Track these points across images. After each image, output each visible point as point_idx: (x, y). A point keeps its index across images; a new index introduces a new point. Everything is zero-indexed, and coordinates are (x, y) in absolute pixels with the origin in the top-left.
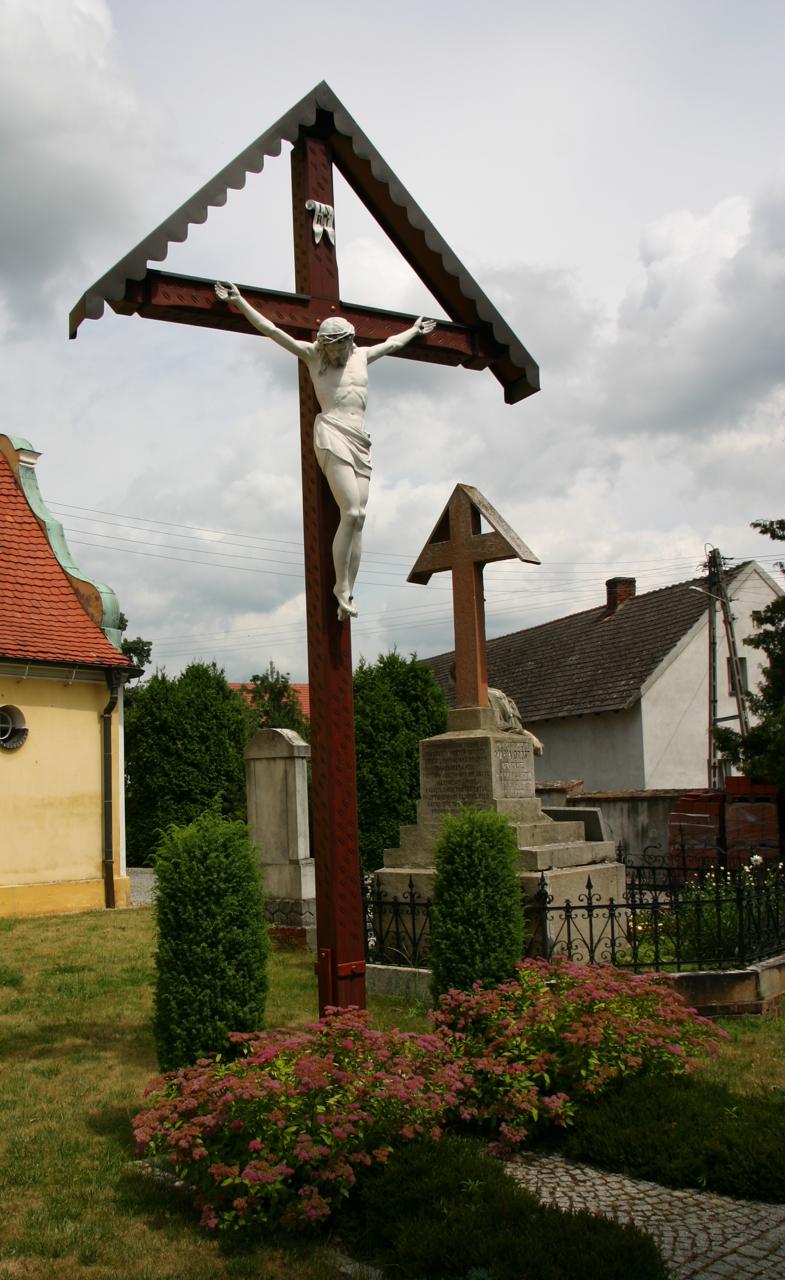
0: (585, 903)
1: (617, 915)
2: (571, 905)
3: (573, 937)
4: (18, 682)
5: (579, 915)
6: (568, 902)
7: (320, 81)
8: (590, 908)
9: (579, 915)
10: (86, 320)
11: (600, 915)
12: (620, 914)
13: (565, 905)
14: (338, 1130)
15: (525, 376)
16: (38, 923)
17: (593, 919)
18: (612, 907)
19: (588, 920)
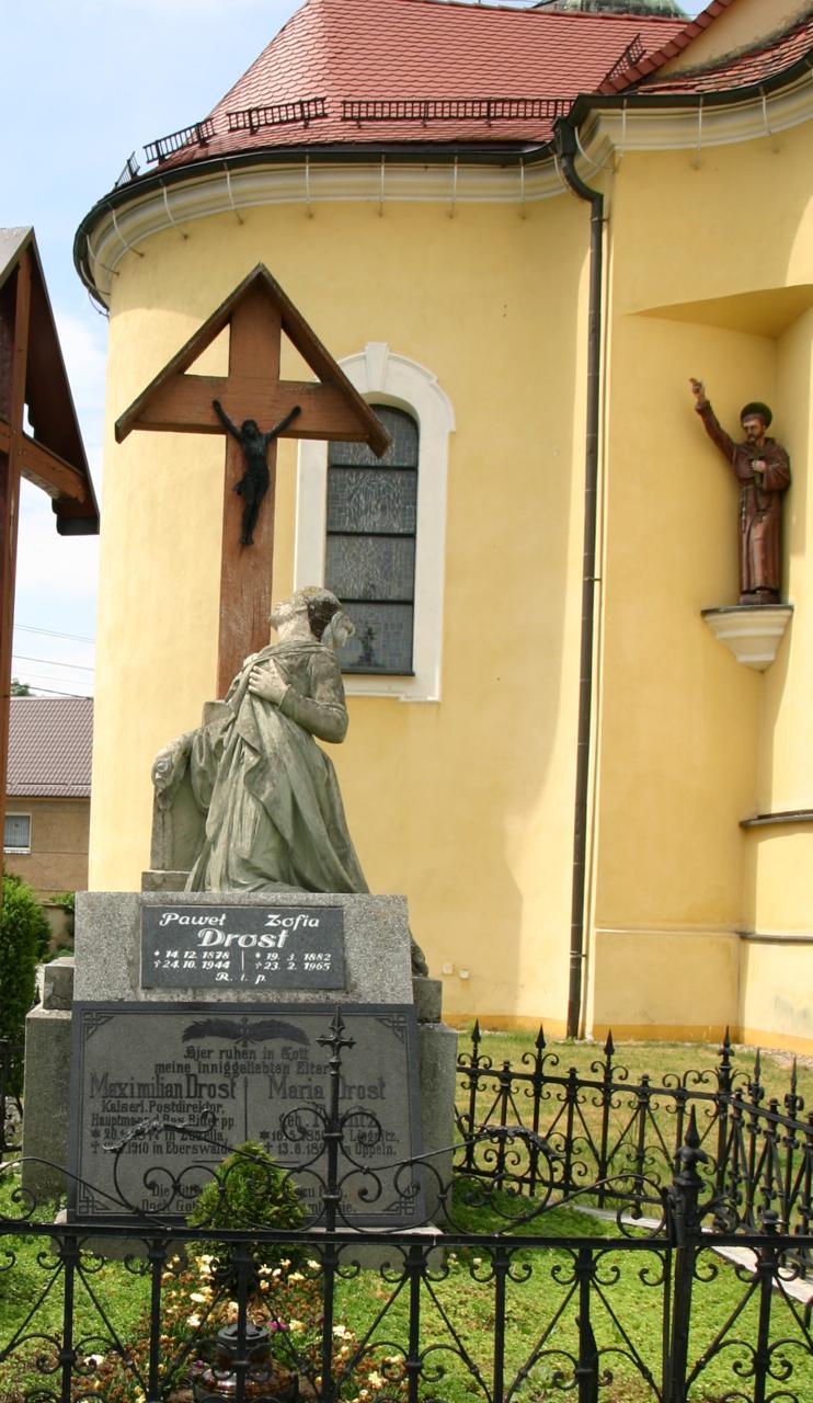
0: (599, 1077)
1: (580, 1099)
2: (512, 1070)
3: (575, 1134)
4: (696, 167)
5: (521, 1090)
6: (573, 1071)
7: (124, 442)
8: (607, 1088)
9: (521, 1090)
10: (134, 431)
11: (553, 1096)
12: (485, 1086)
13: (567, 1076)
14: (317, 1358)
15: (705, 12)
16: (200, 1019)
17: (611, 1111)
18: (506, 1076)
19: (602, 1109)
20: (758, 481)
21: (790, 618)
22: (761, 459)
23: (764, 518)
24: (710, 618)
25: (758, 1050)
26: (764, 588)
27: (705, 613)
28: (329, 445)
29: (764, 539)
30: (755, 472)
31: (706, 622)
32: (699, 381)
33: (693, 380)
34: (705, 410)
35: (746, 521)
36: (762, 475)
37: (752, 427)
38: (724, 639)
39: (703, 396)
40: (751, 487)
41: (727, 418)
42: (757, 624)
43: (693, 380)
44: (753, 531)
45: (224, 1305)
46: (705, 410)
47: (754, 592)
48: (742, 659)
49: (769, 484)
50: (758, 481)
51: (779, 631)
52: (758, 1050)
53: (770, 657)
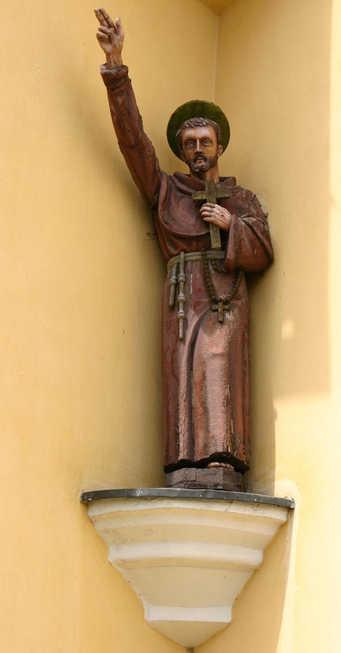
20: (216, 243)
21: (283, 528)
22: (220, 202)
23: (229, 316)
24: (99, 510)
25: (145, 240)
26: (205, 450)
27: (90, 499)
28: (273, 495)
29: (229, 355)
30: (207, 224)
31: (91, 521)
32: (114, 20)
33: (101, 15)
34: (117, 82)
35: (185, 320)
36: (224, 234)
37: (204, 140)
38: (124, 563)
39: (118, 51)
40: (195, 256)
41: (154, 113)
42: (200, 532)
43: (101, 15)
44: (204, 339)
45: (231, 326)
46: (117, 82)
47: (203, 464)
48: (157, 614)
49: (238, 251)
50: (216, 243)
51: (253, 557)
52: (145, 240)
53: (223, 616)
